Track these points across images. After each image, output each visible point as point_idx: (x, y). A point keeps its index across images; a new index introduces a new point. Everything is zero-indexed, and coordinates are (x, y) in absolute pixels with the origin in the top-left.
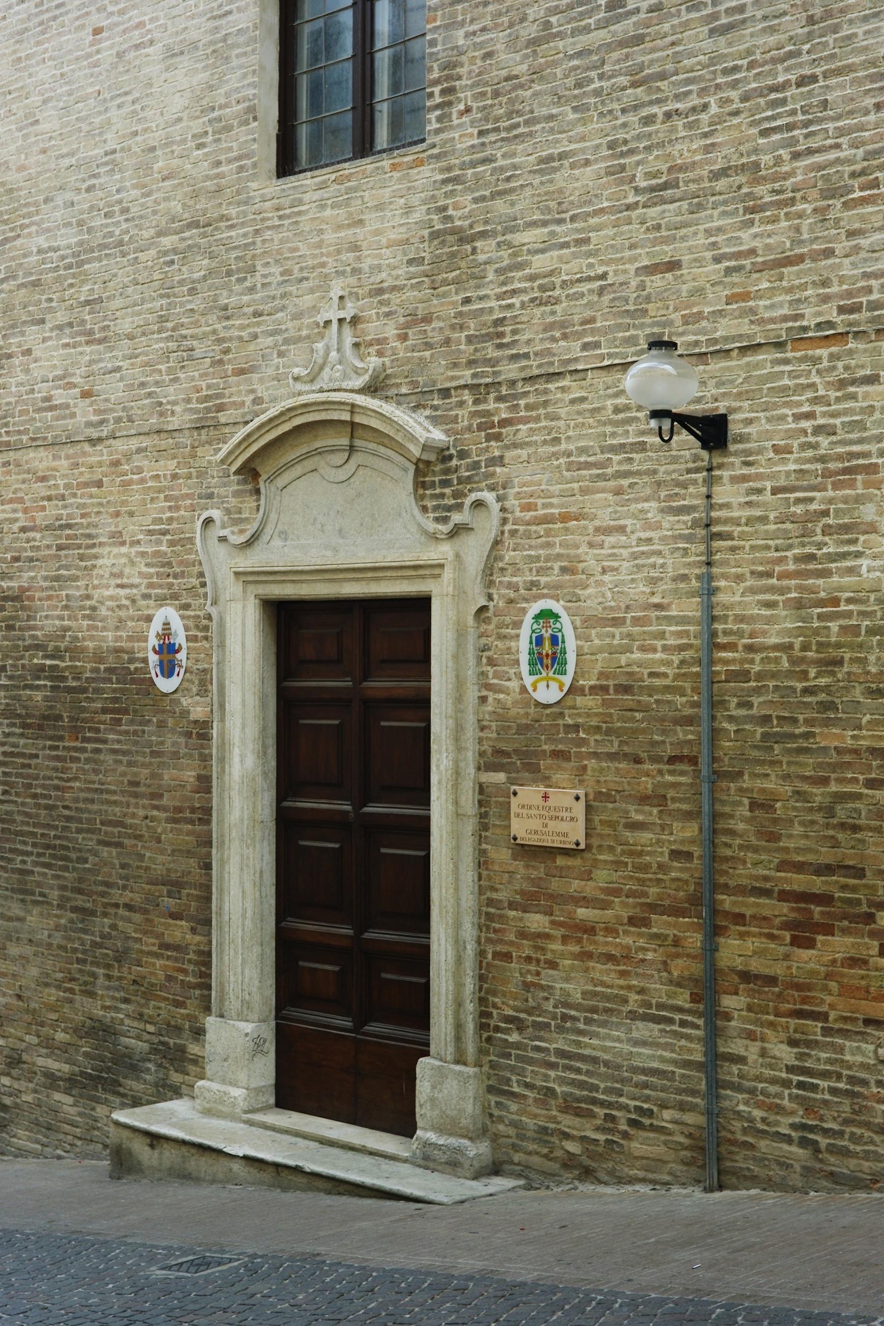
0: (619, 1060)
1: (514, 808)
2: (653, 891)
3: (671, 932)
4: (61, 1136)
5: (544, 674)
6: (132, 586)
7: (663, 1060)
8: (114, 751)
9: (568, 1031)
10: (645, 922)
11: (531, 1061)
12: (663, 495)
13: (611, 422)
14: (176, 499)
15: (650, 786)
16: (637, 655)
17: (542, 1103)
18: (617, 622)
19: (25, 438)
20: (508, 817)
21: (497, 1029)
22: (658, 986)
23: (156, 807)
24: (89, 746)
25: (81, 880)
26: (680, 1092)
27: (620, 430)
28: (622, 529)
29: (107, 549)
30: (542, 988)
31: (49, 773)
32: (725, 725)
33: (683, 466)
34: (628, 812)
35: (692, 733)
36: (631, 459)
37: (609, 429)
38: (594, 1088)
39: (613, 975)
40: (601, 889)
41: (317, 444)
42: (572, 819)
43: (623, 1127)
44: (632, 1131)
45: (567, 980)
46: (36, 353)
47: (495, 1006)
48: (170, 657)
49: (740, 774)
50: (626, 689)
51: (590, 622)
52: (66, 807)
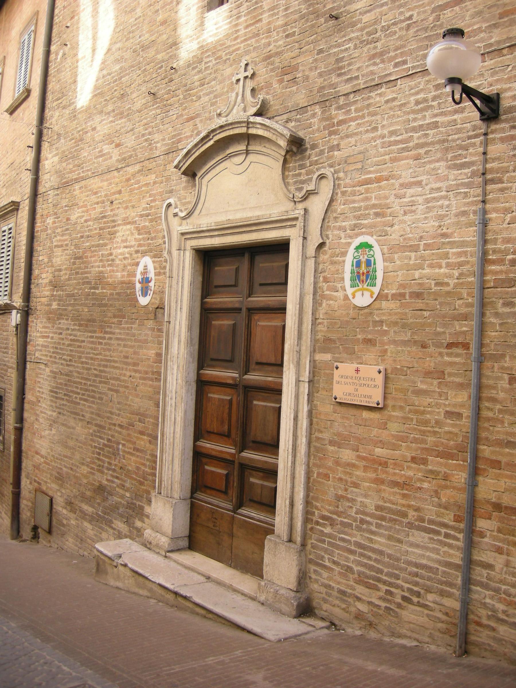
0: (398, 555)
1: (336, 378)
2: (431, 439)
3: (443, 470)
4: (87, 545)
5: (361, 286)
6: (131, 247)
7: (429, 558)
8: (118, 339)
9: (364, 530)
10: (424, 461)
11: (338, 547)
12: (450, 156)
13: (414, 112)
14: (154, 195)
15: (432, 364)
16: (427, 271)
17: (343, 575)
18: (415, 248)
19: (89, 173)
20: (332, 383)
21: (317, 523)
22: (430, 507)
23: (136, 371)
24: (107, 336)
25: (99, 409)
26: (442, 583)
27: (419, 116)
28: (419, 183)
29: (121, 227)
30: (348, 500)
31: (89, 350)
32: (492, 320)
33: (465, 135)
34: (415, 383)
35: (466, 325)
36: (428, 134)
37: (411, 116)
38: (381, 571)
39: (398, 497)
40: (393, 435)
41: (228, 152)
42: (375, 386)
43: (399, 600)
44: (405, 604)
45: (366, 496)
46: (98, 128)
47: (317, 508)
48: (146, 285)
49: (503, 356)
50: (418, 295)
51: (393, 249)
52: (95, 369)
